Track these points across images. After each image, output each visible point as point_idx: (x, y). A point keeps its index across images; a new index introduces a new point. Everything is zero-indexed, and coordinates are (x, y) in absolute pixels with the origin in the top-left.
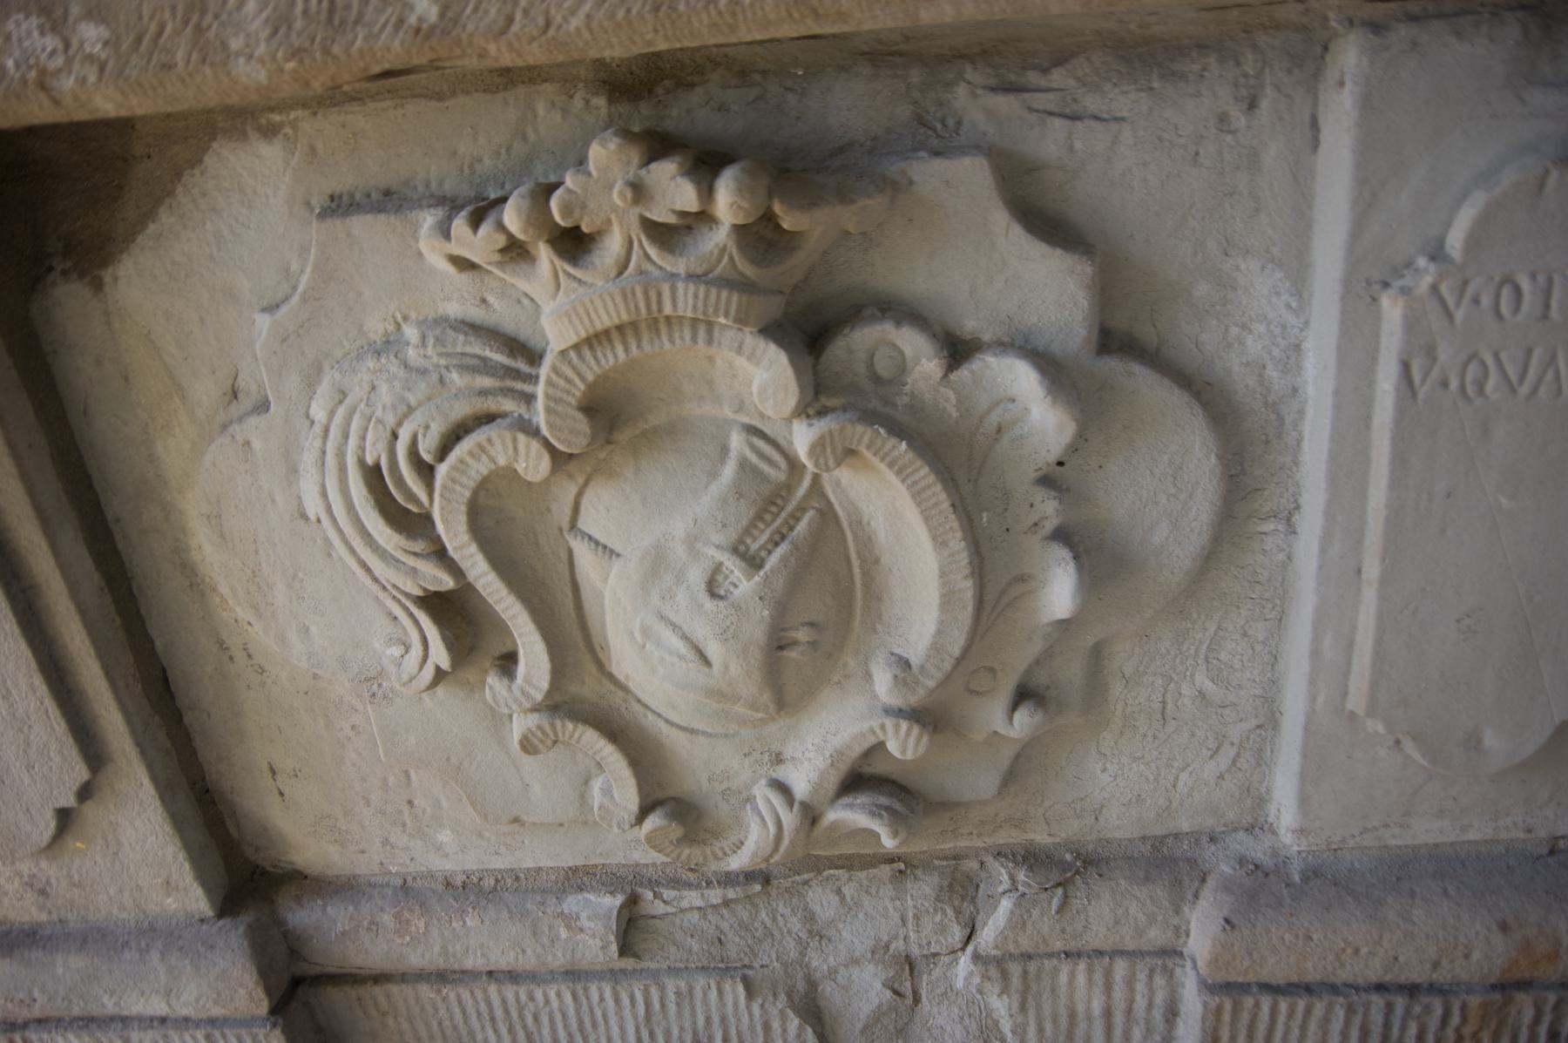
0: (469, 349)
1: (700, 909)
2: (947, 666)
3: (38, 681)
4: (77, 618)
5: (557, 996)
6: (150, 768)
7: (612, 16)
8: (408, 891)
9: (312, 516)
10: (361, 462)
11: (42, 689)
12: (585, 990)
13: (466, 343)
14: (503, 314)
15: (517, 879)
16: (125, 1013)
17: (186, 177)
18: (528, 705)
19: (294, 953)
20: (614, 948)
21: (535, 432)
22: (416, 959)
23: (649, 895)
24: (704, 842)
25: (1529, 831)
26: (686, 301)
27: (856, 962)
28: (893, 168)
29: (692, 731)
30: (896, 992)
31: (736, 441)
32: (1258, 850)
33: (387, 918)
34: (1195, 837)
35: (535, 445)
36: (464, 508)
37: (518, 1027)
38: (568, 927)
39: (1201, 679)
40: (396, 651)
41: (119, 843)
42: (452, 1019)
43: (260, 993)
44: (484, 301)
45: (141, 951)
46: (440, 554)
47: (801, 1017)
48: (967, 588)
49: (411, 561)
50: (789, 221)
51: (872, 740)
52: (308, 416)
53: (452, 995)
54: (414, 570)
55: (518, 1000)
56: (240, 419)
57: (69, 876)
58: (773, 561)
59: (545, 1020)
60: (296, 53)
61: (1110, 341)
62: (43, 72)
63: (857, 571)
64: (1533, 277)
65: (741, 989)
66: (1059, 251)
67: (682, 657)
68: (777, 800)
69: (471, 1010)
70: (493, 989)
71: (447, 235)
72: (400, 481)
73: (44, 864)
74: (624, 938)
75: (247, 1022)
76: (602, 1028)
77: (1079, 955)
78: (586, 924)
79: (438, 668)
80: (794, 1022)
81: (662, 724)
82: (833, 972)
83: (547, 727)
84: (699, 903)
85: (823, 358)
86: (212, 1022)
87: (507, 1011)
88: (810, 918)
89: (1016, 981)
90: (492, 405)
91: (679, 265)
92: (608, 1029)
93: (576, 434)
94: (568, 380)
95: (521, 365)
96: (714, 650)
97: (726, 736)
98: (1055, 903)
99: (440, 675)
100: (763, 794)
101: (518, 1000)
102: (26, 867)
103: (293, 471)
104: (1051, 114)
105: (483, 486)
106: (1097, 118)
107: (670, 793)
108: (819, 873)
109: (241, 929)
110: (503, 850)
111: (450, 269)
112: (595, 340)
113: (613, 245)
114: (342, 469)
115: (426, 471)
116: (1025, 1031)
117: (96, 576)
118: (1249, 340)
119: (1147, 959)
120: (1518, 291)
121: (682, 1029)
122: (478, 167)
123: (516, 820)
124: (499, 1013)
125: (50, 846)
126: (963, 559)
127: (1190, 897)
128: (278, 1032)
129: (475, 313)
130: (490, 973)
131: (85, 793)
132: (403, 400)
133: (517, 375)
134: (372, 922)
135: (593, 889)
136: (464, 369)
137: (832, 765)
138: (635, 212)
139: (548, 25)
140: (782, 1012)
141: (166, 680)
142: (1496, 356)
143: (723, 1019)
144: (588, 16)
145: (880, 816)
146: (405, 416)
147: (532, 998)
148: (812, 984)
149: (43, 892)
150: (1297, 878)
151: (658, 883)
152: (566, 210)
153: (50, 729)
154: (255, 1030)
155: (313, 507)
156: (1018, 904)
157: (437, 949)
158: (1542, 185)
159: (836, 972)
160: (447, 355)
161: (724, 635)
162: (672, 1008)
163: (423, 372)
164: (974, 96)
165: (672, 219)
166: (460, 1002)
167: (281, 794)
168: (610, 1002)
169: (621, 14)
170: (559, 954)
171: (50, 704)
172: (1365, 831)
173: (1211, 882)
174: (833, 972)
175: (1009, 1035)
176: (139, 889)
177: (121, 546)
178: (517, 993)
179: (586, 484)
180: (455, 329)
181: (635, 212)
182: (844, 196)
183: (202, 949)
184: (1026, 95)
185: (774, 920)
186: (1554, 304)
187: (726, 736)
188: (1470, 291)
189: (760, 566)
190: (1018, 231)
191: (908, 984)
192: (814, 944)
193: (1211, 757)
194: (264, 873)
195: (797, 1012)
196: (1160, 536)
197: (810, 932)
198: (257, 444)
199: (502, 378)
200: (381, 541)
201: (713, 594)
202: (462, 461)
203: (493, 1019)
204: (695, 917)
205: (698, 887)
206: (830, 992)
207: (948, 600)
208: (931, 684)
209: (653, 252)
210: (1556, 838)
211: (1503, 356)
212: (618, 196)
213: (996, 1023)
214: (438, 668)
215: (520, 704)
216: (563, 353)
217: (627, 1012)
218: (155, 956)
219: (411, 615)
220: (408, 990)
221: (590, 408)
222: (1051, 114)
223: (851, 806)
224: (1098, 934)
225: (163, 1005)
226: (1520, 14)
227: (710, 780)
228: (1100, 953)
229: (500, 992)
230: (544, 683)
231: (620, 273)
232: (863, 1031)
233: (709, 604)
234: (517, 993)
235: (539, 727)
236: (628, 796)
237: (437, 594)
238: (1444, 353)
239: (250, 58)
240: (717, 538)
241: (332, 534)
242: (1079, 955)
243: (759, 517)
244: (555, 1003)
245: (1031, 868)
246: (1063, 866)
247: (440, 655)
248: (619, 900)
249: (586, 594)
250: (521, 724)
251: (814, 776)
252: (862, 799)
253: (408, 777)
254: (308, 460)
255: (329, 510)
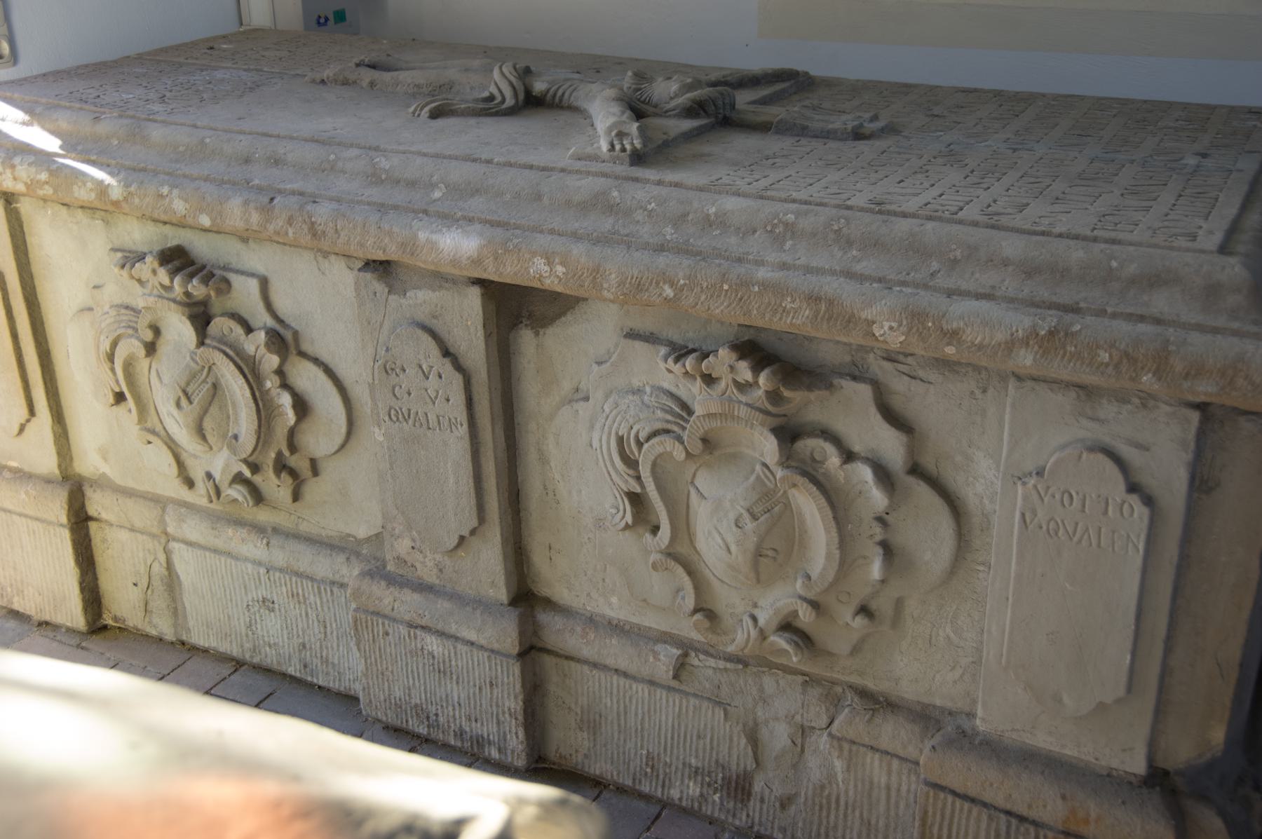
0: (667, 403)
1: (713, 668)
2: (826, 584)
3: (471, 481)
4: (493, 460)
5: (641, 690)
6: (502, 529)
7: (730, 313)
8: (592, 621)
9: (594, 447)
10: (617, 433)
11: (472, 484)
12: (655, 691)
13: (666, 400)
14: (682, 393)
15: (640, 629)
16: (459, 635)
17: (580, 304)
18: (658, 549)
19: (535, 633)
20: (671, 673)
21: (682, 443)
22: (586, 652)
23: (693, 654)
24: (718, 634)
25: (1097, 759)
26: (743, 411)
27: (777, 719)
28: (836, 381)
29: (722, 581)
30: (793, 742)
31: (758, 467)
32: (966, 725)
33: (579, 629)
34: (943, 710)
35: (681, 447)
36: (650, 463)
37: (622, 702)
38: (654, 657)
39: (948, 630)
40: (614, 511)
41: (479, 559)
42: (594, 687)
43: (517, 643)
44: (677, 386)
45: (473, 609)
46: (638, 478)
47: (747, 739)
48: (837, 553)
49: (626, 477)
50: (786, 393)
51: (792, 608)
52: (602, 408)
53: (597, 675)
54: (627, 481)
55: (625, 687)
56: (577, 401)
57: (454, 566)
58: (762, 519)
59: (634, 702)
60: (624, 294)
61: (915, 470)
62: (541, 276)
63: (797, 534)
64: (1077, 493)
65: (722, 713)
66: (893, 429)
67: (720, 547)
68: (750, 623)
69: (603, 685)
70: (615, 677)
71: (666, 361)
72: (629, 445)
73: (446, 558)
74: (677, 671)
75: (507, 656)
76: (658, 714)
77: (878, 750)
78: (662, 657)
79: (627, 523)
80: (744, 741)
81: (711, 575)
82: (767, 722)
83: (664, 561)
84: (713, 665)
85: (795, 445)
86: (492, 651)
87: (618, 691)
88: (761, 690)
89: (846, 753)
90: (669, 427)
91: (743, 399)
92: (661, 715)
93: (697, 447)
94: (698, 427)
95: (684, 415)
96: (733, 548)
97: (736, 588)
98: (867, 717)
99: (627, 527)
100: (748, 621)
101: (625, 687)
102: (438, 557)
103: (592, 427)
104: (904, 373)
105: (660, 455)
106: (922, 380)
107: (709, 607)
108: (771, 669)
109: (517, 613)
110: (637, 613)
111: (664, 370)
112: (710, 416)
113: (723, 384)
114: (610, 434)
115: (640, 444)
116: (848, 784)
117: (504, 444)
118: (977, 484)
119: (908, 763)
120: (1071, 496)
121: (693, 726)
122: (687, 334)
123: (645, 600)
124: (615, 691)
125: (451, 551)
126: (836, 540)
127: (929, 736)
128: (518, 664)
129: (674, 390)
130: (616, 670)
131: (473, 532)
132: (638, 415)
133: (682, 418)
134: (572, 629)
135: (670, 644)
136: (663, 410)
137: (775, 614)
138: (730, 376)
139: (709, 309)
140: (739, 733)
141: (518, 494)
142: (1063, 522)
143: (712, 728)
144: (722, 311)
145: (791, 644)
146: (637, 421)
147: (631, 688)
148: (756, 724)
149: (441, 570)
150: (977, 742)
151: (699, 651)
152: (707, 368)
153: (469, 501)
154: (509, 660)
155: (596, 444)
156: (851, 712)
157: (596, 650)
158: (1080, 457)
159: (768, 722)
160: (659, 403)
161: (738, 543)
162: (691, 713)
163: (648, 407)
164: (876, 359)
165: (743, 382)
166: (599, 679)
167: (551, 559)
168: (664, 701)
169: (733, 313)
170: (647, 668)
171: (472, 491)
172: (1013, 730)
173: (941, 733)
174: (767, 722)
175: (841, 783)
176: (480, 581)
177: (517, 434)
178: (625, 683)
179: (700, 466)
180: (664, 393)
181: (730, 376)
182: (810, 388)
183: (498, 616)
184: (896, 364)
185: (746, 686)
186: (1087, 506)
187: (736, 588)
188: (1050, 491)
189: (757, 520)
190: (879, 417)
191: (800, 740)
192: (761, 704)
193: (951, 670)
194: (533, 594)
195: (746, 736)
196: (928, 556)
197: (760, 697)
198: (580, 412)
199: (676, 418)
200: (617, 466)
201: (737, 526)
202: (653, 445)
203: (611, 693)
204: (710, 672)
205: (715, 658)
206: (764, 733)
207: (829, 556)
208: (818, 590)
209: (735, 391)
210: (1111, 769)
211: (1066, 522)
212: (725, 369)
213: (836, 774)
214: (627, 523)
215: (655, 548)
216: (698, 416)
217: (670, 709)
218: (478, 612)
219: (622, 498)
220: (579, 666)
221: (705, 441)
222: (904, 373)
223: (780, 636)
224: (885, 743)
225: (476, 636)
226: (1077, 389)
227: (726, 606)
228: (887, 753)
229: (618, 681)
230: (666, 541)
231: (722, 395)
232: (776, 758)
233: (734, 529)
234: (625, 683)
235: (660, 560)
236: (690, 603)
237: (633, 493)
238: (1040, 514)
239: (609, 291)
240: (742, 503)
241: (600, 456)
242: (878, 750)
243: (760, 499)
244: (640, 694)
245: (861, 698)
246: (877, 702)
247: (629, 518)
248: (679, 652)
249: (691, 511)
250: (654, 557)
251: (767, 617)
252: (786, 635)
253: (606, 568)
254: (598, 426)
255: (601, 447)
